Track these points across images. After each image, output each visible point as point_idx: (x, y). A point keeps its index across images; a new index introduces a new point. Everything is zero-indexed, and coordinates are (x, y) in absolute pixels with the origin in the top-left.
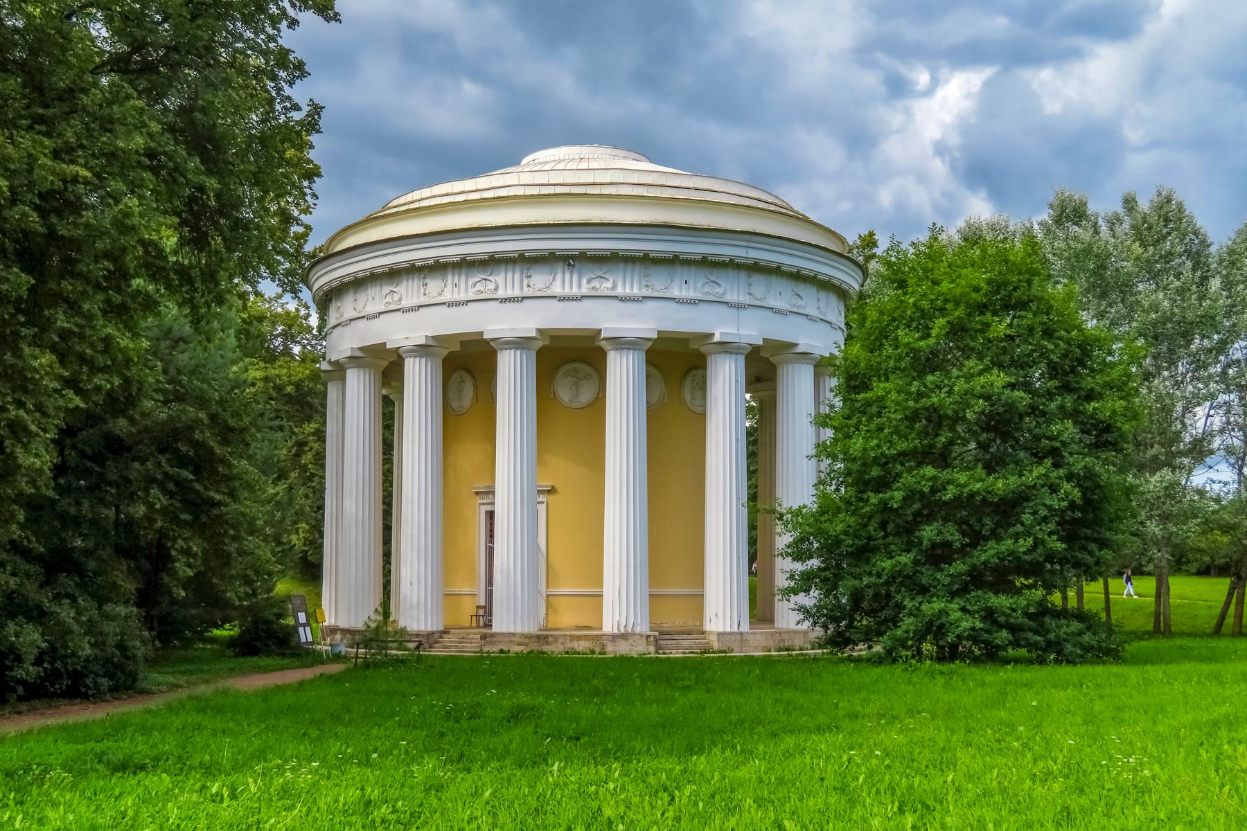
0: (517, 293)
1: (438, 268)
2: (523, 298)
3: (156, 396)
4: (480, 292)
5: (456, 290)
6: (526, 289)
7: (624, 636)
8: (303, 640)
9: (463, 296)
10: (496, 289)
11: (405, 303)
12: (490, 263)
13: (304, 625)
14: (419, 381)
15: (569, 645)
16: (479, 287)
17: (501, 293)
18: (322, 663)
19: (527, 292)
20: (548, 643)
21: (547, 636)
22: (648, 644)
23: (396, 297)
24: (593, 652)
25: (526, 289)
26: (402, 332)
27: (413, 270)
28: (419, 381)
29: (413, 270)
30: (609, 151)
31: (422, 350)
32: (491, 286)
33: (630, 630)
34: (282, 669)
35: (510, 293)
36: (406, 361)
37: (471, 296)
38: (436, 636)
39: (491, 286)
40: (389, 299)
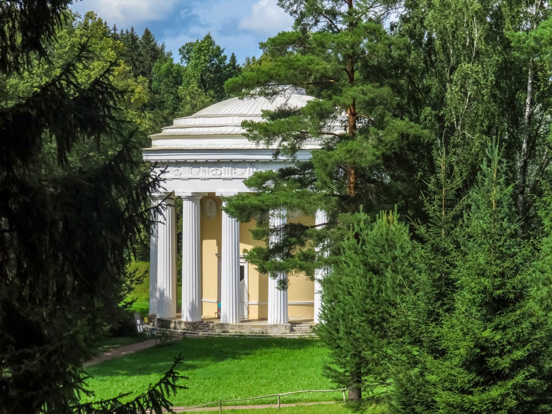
0: (230, 176)
1: (195, 164)
2: (233, 179)
3: (53, 39)
4: (214, 175)
5: (204, 173)
6: (234, 174)
7: (275, 326)
8: (139, 331)
9: (207, 176)
10: (221, 174)
11: (183, 176)
12: (218, 163)
13: (139, 325)
14: (189, 211)
15: (252, 329)
16: (214, 172)
17: (223, 176)
18: (146, 340)
19: (234, 176)
20: (243, 329)
21: (242, 326)
22: (286, 329)
23: (179, 173)
24: (263, 333)
25: (234, 174)
26: (182, 189)
27: (185, 163)
28: (189, 211)
29: (185, 163)
30: (100, 378)
31: (189, 198)
32: (219, 172)
33: (278, 323)
34: (131, 344)
35: (227, 176)
36: (184, 202)
37: (211, 176)
38: (197, 324)
39: (219, 172)
40: (176, 173)
